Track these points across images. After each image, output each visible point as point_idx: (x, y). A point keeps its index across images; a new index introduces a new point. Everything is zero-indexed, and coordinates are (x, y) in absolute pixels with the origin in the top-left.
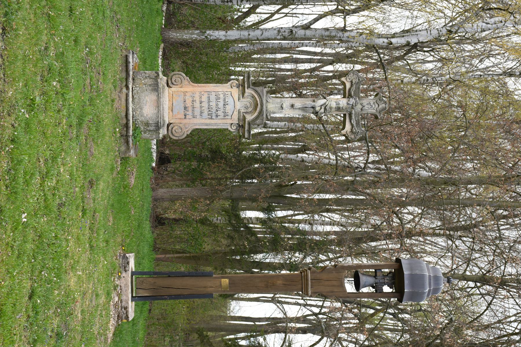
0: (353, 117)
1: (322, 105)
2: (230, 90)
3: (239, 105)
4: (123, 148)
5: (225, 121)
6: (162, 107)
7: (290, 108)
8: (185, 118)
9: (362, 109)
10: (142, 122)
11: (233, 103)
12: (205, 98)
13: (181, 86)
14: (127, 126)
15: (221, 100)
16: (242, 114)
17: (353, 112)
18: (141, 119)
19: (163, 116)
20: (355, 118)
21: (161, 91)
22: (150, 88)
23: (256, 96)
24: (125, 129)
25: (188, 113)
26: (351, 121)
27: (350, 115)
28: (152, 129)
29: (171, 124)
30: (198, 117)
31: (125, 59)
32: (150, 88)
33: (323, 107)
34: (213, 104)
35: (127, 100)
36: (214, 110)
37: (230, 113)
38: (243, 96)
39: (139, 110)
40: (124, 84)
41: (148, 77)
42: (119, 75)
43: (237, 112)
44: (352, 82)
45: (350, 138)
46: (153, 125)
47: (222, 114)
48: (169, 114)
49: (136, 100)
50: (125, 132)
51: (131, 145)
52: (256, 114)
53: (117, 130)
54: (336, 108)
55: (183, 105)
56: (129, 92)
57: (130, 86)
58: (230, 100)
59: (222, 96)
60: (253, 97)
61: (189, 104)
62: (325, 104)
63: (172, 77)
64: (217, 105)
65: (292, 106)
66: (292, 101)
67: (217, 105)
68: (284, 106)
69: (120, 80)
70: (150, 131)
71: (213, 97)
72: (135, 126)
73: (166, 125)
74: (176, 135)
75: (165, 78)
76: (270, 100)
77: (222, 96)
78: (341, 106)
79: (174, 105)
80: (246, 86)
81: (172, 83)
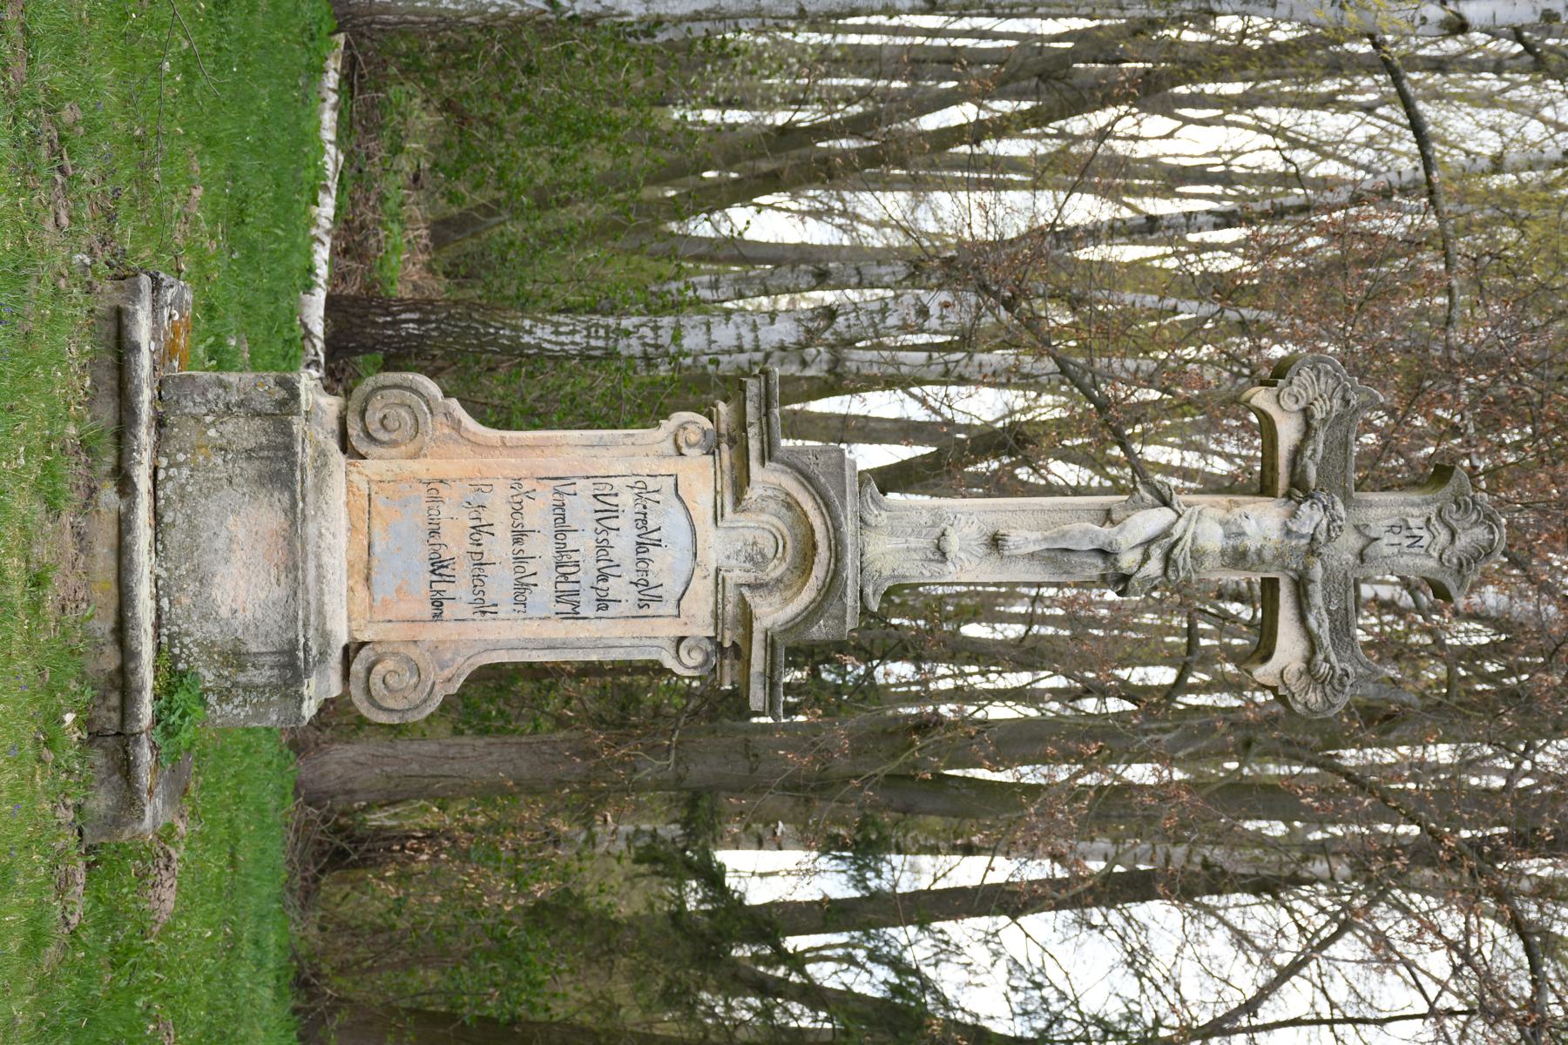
0: (1317, 598)
1: (1149, 542)
2: (672, 465)
3: (717, 547)
4: (101, 802)
5: (642, 627)
6: (311, 565)
7: (982, 550)
8: (437, 617)
9: (1361, 556)
10: (207, 647)
11: (685, 538)
12: (537, 515)
13: (412, 447)
14: (122, 682)
15: (626, 523)
16: (731, 595)
17: (1317, 572)
18: (199, 631)
19: (321, 613)
20: (1327, 600)
21: (310, 481)
22: (251, 470)
23: (808, 505)
24: (114, 700)
25: (450, 590)
26: (1303, 619)
27: (1301, 587)
28: (259, 680)
29: (363, 644)
30: (505, 609)
31: (110, 328)
32: (251, 470)
33: (1156, 553)
34: (583, 542)
35: (122, 551)
36: (587, 575)
37: (672, 589)
38: (738, 500)
39: (192, 587)
40: (109, 460)
41: (241, 404)
42: (79, 421)
43: (710, 582)
44: (1306, 413)
45: (1298, 708)
46: (269, 660)
47: (632, 594)
48: (350, 601)
49: (175, 537)
50: (115, 717)
51: (145, 778)
52: (807, 596)
53: (69, 718)
54: (1223, 553)
55: (424, 552)
56: (131, 508)
57: (143, 481)
58: (669, 521)
59: (626, 500)
60: (791, 504)
61: (455, 543)
62: (1166, 533)
63: (367, 400)
64: (603, 547)
65: (995, 542)
66: (990, 518)
67: (603, 547)
68: (953, 544)
69: (85, 446)
70: (248, 688)
71: (581, 509)
72: (172, 671)
73: (336, 655)
74: (390, 703)
75: (330, 405)
76: (874, 515)
77: (626, 500)
78: (1252, 544)
79: (377, 549)
80: (754, 446)
81: (368, 435)
